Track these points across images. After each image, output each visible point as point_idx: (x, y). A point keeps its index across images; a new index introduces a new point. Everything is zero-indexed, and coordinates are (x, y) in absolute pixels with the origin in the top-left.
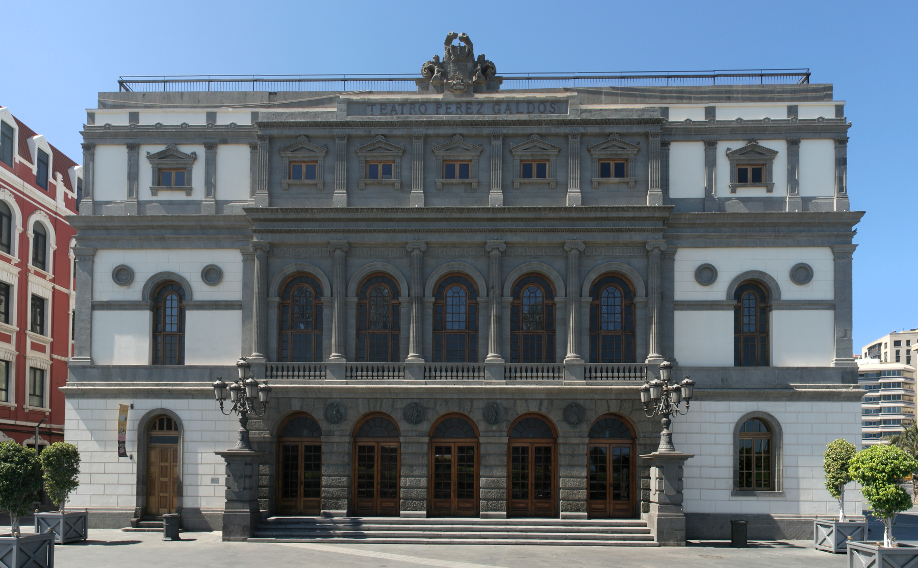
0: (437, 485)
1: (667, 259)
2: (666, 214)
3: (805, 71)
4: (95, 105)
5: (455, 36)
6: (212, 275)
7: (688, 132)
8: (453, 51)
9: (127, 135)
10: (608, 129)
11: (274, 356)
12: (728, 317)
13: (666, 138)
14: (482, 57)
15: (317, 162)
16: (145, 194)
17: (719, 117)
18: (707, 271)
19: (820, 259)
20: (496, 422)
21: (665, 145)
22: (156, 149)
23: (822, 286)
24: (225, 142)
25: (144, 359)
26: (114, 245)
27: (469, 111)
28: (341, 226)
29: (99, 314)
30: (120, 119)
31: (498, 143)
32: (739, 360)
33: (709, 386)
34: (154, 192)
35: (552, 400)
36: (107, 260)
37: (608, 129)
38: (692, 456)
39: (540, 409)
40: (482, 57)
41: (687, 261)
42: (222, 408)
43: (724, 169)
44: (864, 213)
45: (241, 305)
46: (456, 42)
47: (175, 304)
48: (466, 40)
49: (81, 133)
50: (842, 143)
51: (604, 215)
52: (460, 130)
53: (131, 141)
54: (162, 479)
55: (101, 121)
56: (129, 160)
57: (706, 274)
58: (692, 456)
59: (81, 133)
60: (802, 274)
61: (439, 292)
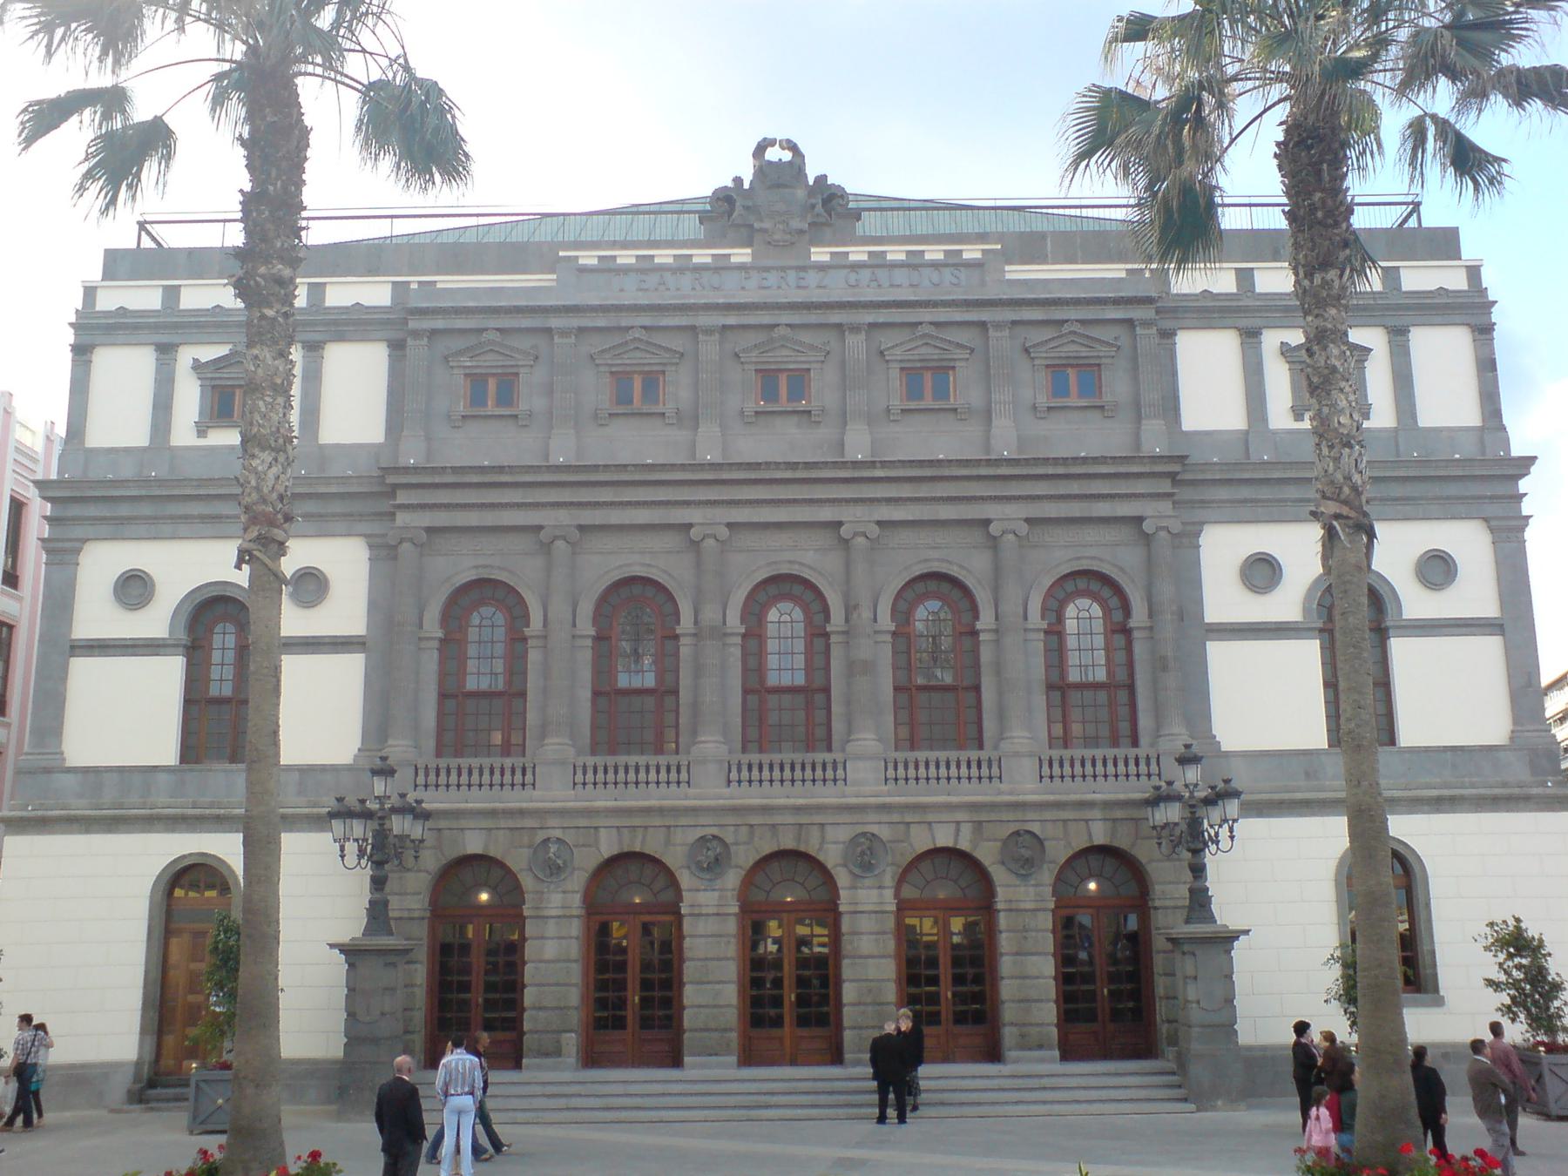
0: (756, 1002)
1: (1188, 539)
2: (1176, 468)
3: (1410, 199)
4: (95, 273)
5: (772, 143)
6: (1437, 569)
7: (1209, 312)
8: (765, 170)
9: (157, 328)
10: (1058, 314)
11: (430, 744)
12: (171, 671)
13: (1167, 324)
14: (821, 179)
15: (517, 374)
16: (183, 433)
17: (1261, 287)
18: (1250, 571)
19: (1467, 541)
20: (867, 867)
21: (1168, 335)
22: (209, 353)
23: (1475, 593)
24: (341, 338)
25: (163, 747)
26: (119, 528)
27: (802, 283)
28: (566, 495)
29: (81, 667)
30: (144, 297)
31: (744, 830)
32: (192, 749)
33: (1283, 789)
34: (201, 431)
35: (980, 823)
36: (102, 563)
37: (1058, 314)
38: (1247, 932)
39: (956, 841)
40: (821, 179)
41: (1223, 548)
42: (342, 857)
43: (189, 398)
44: (1535, 458)
45: (364, 644)
46: (773, 154)
47: (231, 641)
48: (792, 147)
49: (71, 324)
50: (1484, 331)
51: (1061, 470)
52: (786, 318)
53: (164, 338)
54: (191, 998)
55: (108, 301)
56: (158, 371)
57: (1261, 572)
58: (1247, 932)
59: (71, 324)
60: (1437, 569)
61: (755, 610)
